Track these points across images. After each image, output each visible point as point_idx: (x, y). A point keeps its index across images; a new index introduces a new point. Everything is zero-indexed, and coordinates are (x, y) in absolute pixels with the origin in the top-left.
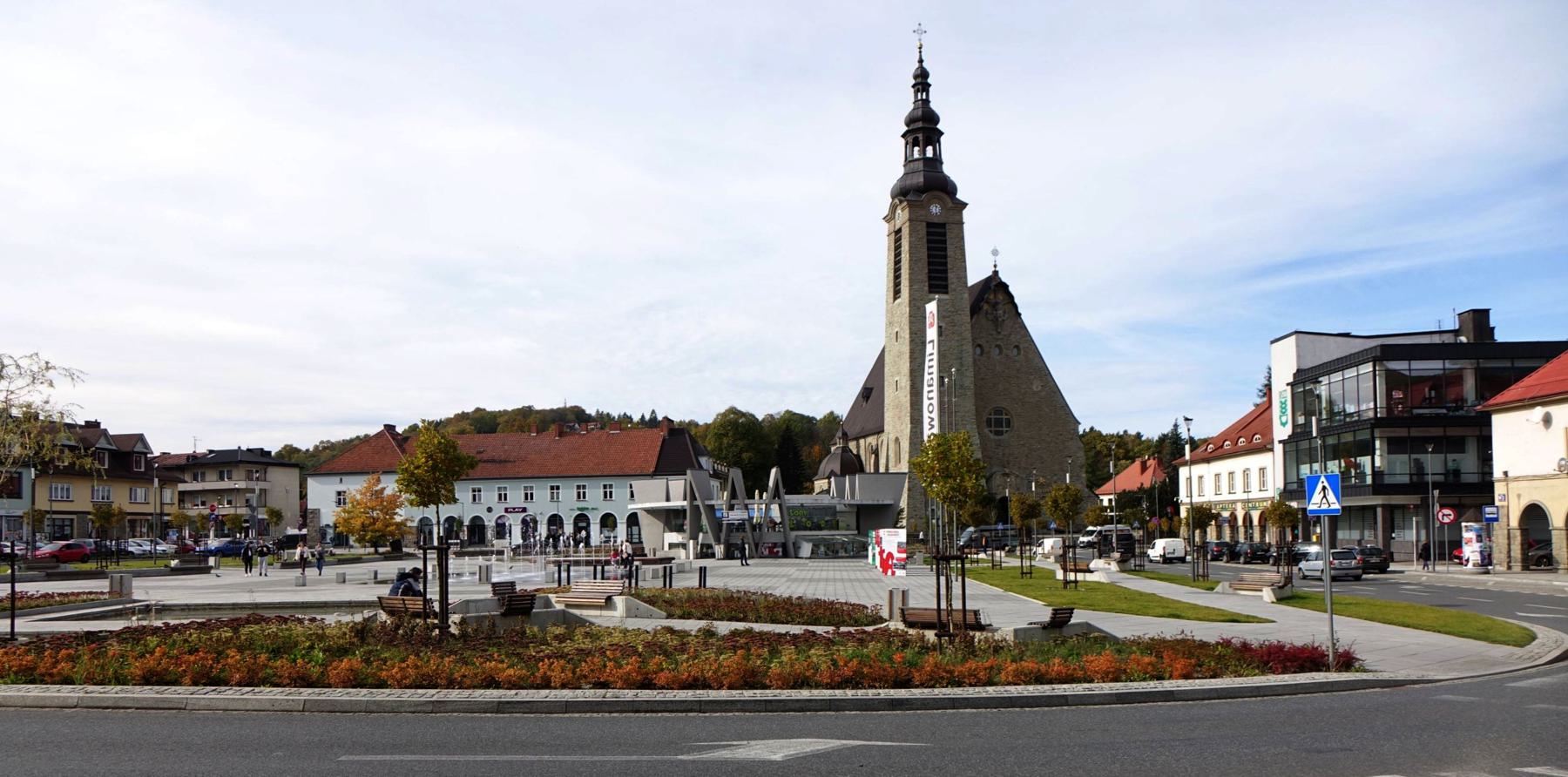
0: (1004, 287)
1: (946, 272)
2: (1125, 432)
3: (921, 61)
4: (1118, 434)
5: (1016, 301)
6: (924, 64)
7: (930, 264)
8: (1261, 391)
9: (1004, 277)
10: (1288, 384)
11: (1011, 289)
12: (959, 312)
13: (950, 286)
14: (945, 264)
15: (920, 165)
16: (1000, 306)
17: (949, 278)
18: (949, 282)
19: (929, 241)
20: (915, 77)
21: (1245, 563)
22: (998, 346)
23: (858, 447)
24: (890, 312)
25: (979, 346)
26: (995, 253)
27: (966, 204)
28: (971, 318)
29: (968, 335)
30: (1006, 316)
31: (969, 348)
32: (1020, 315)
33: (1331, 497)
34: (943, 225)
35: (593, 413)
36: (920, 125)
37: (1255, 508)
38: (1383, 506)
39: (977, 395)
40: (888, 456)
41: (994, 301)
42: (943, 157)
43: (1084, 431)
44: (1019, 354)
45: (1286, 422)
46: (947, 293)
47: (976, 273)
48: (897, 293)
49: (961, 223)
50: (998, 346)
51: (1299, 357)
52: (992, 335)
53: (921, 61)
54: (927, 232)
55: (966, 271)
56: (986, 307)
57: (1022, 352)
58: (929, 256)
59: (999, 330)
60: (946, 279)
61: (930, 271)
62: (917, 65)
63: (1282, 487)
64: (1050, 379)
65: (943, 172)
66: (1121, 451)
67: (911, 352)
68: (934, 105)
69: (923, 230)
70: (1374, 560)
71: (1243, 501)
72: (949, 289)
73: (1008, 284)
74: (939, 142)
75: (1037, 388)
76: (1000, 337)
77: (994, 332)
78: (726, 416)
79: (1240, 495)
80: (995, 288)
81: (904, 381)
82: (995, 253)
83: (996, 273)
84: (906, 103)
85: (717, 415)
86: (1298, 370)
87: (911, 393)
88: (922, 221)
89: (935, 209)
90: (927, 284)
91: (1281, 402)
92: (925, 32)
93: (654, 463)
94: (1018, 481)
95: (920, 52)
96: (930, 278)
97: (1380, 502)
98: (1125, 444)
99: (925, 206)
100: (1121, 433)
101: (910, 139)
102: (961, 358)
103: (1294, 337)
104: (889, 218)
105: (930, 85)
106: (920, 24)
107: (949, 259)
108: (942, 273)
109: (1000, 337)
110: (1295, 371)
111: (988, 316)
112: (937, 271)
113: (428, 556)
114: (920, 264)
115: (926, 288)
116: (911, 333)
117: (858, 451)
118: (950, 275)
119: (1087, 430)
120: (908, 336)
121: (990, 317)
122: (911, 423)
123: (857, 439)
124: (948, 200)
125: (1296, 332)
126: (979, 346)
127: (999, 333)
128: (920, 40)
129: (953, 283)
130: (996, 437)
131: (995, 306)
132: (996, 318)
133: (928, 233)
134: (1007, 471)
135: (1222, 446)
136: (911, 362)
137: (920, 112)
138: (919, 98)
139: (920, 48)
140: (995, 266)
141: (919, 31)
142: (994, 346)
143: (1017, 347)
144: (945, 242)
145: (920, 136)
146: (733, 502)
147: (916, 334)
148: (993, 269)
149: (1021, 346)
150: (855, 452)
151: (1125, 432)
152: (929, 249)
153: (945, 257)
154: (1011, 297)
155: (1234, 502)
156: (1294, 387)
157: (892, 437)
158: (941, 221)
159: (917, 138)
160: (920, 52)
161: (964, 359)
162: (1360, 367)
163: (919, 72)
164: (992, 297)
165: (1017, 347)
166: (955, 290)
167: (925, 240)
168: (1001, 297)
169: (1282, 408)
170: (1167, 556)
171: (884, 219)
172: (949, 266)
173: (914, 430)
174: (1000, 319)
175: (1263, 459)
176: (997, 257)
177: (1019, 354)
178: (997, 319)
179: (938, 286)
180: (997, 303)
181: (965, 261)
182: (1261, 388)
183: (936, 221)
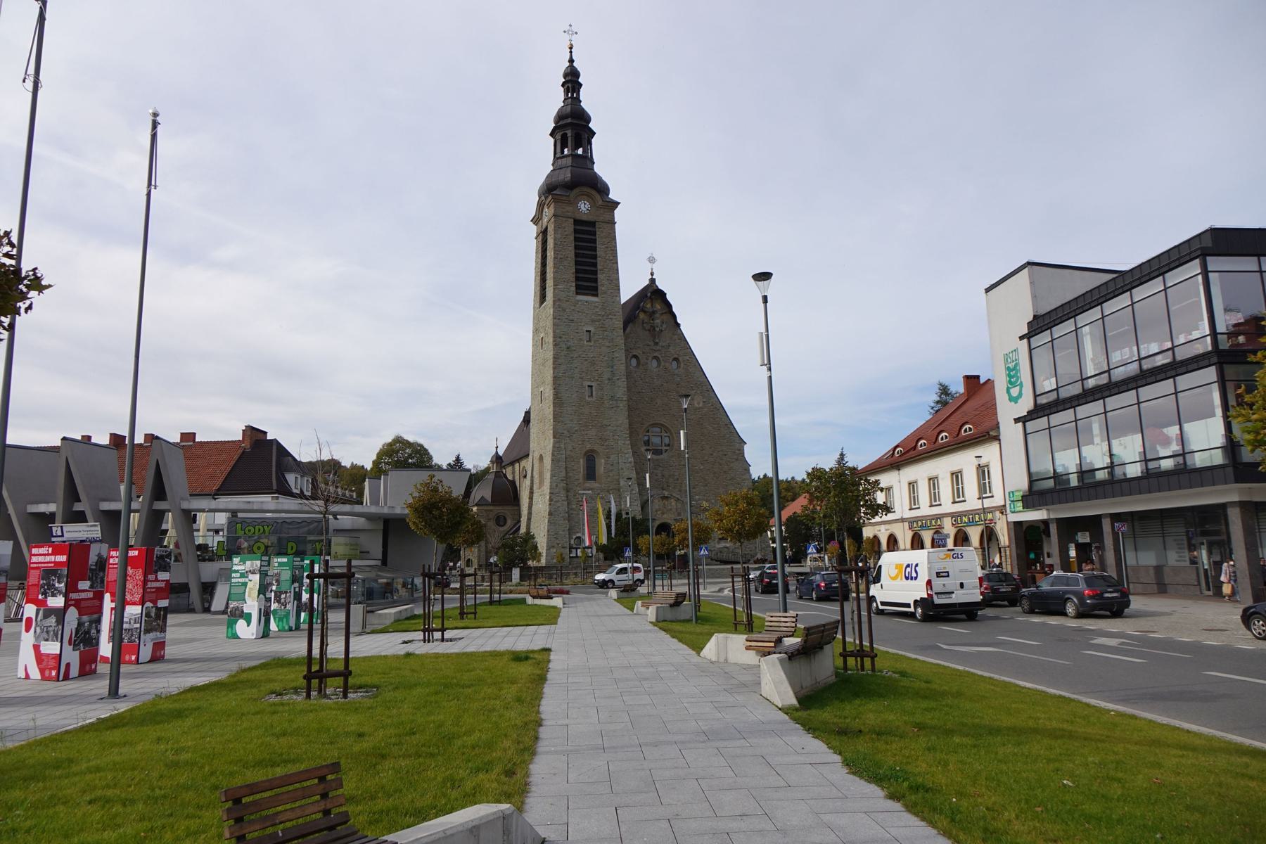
0: (661, 295)
1: (595, 273)
2: (793, 478)
3: (571, 61)
4: (786, 480)
5: (674, 310)
6: (575, 64)
7: (577, 263)
8: (932, 408)
9: (660, 285)
10: (1021, 338)
11: (668, 297)
12: (610, 317)
13: (599, 288)
14: (595, 265)
15: (569, 161)
16: (657, 315)
17: (599, 280)
18: (599, 284)
19: (576, 239)
20: (565, 76)
21: (1080, 615)
22: (655, 358)
23: (514, 473)
24: (537, 319)
25: (635, 356)
26: (652, 260)
27: (619, 203)
28: (625, 329)
29: (620, 341)
30: (664, 326)
31: (621, 355)
32: (678, 325)
33: (814, 550)
34: (593, 224)
35: (348, 465)
36: (569, 120)
37: (972, 523)
38: (1242, 505)
39: (630, 409)
40: (532, 477)
41: (651, 310)
42: (594, 157)
43: (759, 478)
44: (678, 367)
45: (1020, 395)
46: (596, 295)
47: (630, 286)
48: (543, 298)
49: (612, 223)
50: (655, 358)
51: (1034, 297)
52: (648, 345)
53: (571, 61)
54: (575, 229)
55: (618, 273)
56: (642, 316)
57: (682, 365)
58: (576, 255)
59: (657, 341)
60: (596, 280)
61: (577, 271)
62: (568, 64)
63: (1024, 485)
64: (713, 395)
65: (593, 169)
66: (790, 494)
67: (554, 358)
68: (586, 104)
69: (570, 227)
70: (1004, 588)
71: (953, 515)
72: (599, 291)
73: (665, 292)
74: (590, 143)
75: (699, 403)
76: (658, 348)
77: (651, 343)
78: (391, 446)
79: (947, 506)
80: (653, 296)
81: (548, 390)
82: (652, 260)
83: (653, 281)
84: (557, 99)
85: (383, 446)
86: (1035, 317)
87: (554, 403)
88: (571, 218)
89: (584, 206)
90: (574, 284)
91: (1008, 369)
92: (576, 33)
93: (221, 480)
94: (679, 505)
95: (571, 52)
96: (577, 279)
97: (1236, 498)
98: (793, 488)
99: (574, 203)
100: (790, 479)
101: (558, 136)
102: (612, 367)
103: (1026, 270)
104: (535, 221)
105: (581, 85)
106: (570, 25)
107: (599, 259)
108: (592, 274)
109: (658, 348)
110: (1031, 318)
111: (645, 325)
112: (586, 272)
113: (735, 580)
114: (566, 263)
115: (573, 289)
116: (555, 337)
117: (514, 477)
118: (600, 276)
119: (762, 477)
120: (551, 340)
121: (647, 327)
122: (554, 437)
123: (512, 464)
124: (598, 197)
125: (1029, 264)
126: (635, 356)
127: (657, 344)
128: (570, 40)
129: (603, 285)
130: (655, 457)
131: (652, 314)
132: (653, 328)
133: (576, 231)
134: (666, 493)
135: (915, 448)
136: (554, 368)
137: (569, 108)
138: (569, 96)
139: (571, 48)
140: (652, 269)
141: (570, 31)
142: (650, 358)
143: (676, 359)
144: (594, 241)
145: (569, 133)
146: (160, 505)
147: (560, 337)
148: (651, 277)
149: (680, 359)
150: (510, 478)
151: (793, 478)
152: (576, 247)
153: (595, 257)
154: (669, 306)
155: (940, 517)
156: (1032, 339)
157: (537, 455)
158: (591, 218)
159: (566, 134)
160: (571, 52)
161: (615, 367)
162: (1167, 275)
163: (569, 70)
164: (649, 306)
165: (676, 359)
166: (605, 293)
167: (572, 238)
168: (658, 306)
169: (1010, 377)
170: (937, 601)
171: (532, 221)
172: (599, 267)
173: (557, 445)
174: (657, 329)
175: (989, 453)
176: (654, 265)
177: (678, 367)
178: (654, 329)
179: (587, 288)
180: (654, 312)
181: (617, 263)
182: (933, 405)
183: (585, 218)
